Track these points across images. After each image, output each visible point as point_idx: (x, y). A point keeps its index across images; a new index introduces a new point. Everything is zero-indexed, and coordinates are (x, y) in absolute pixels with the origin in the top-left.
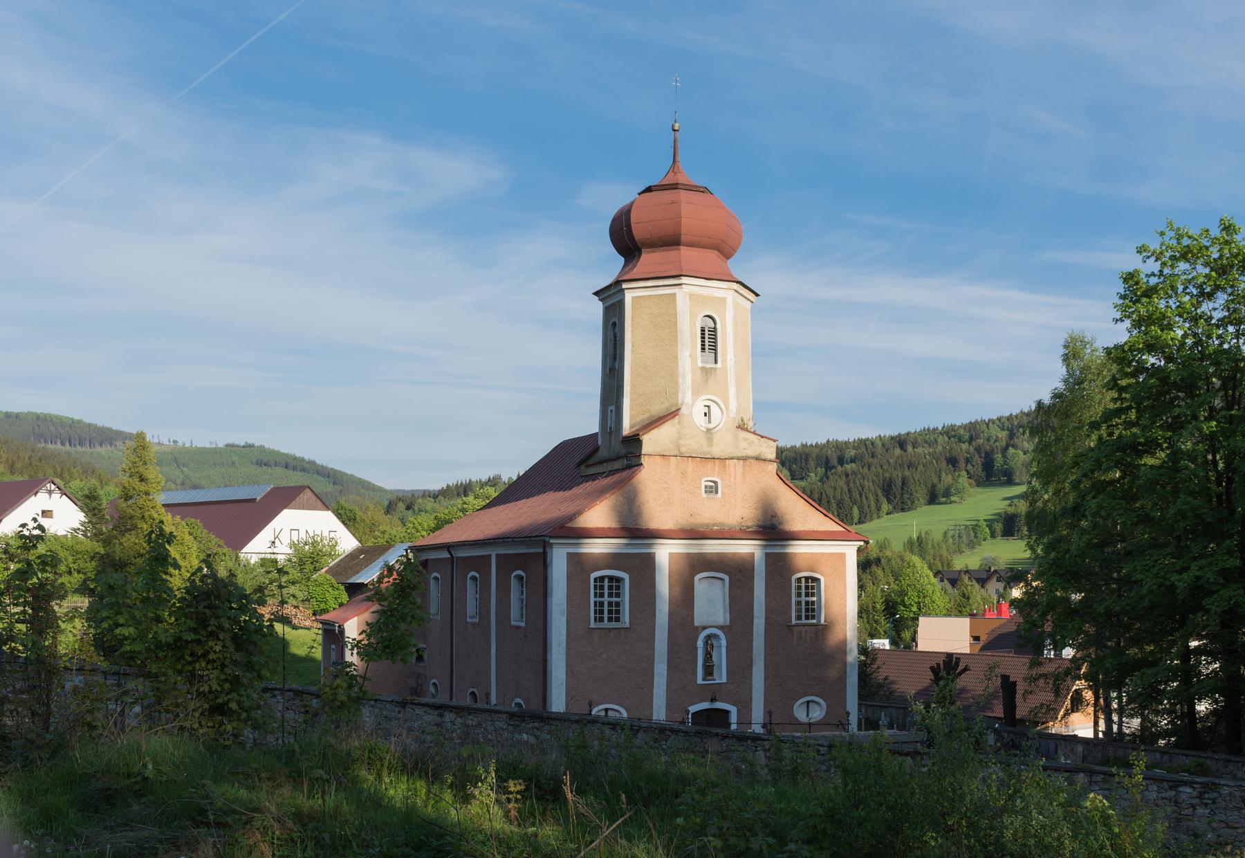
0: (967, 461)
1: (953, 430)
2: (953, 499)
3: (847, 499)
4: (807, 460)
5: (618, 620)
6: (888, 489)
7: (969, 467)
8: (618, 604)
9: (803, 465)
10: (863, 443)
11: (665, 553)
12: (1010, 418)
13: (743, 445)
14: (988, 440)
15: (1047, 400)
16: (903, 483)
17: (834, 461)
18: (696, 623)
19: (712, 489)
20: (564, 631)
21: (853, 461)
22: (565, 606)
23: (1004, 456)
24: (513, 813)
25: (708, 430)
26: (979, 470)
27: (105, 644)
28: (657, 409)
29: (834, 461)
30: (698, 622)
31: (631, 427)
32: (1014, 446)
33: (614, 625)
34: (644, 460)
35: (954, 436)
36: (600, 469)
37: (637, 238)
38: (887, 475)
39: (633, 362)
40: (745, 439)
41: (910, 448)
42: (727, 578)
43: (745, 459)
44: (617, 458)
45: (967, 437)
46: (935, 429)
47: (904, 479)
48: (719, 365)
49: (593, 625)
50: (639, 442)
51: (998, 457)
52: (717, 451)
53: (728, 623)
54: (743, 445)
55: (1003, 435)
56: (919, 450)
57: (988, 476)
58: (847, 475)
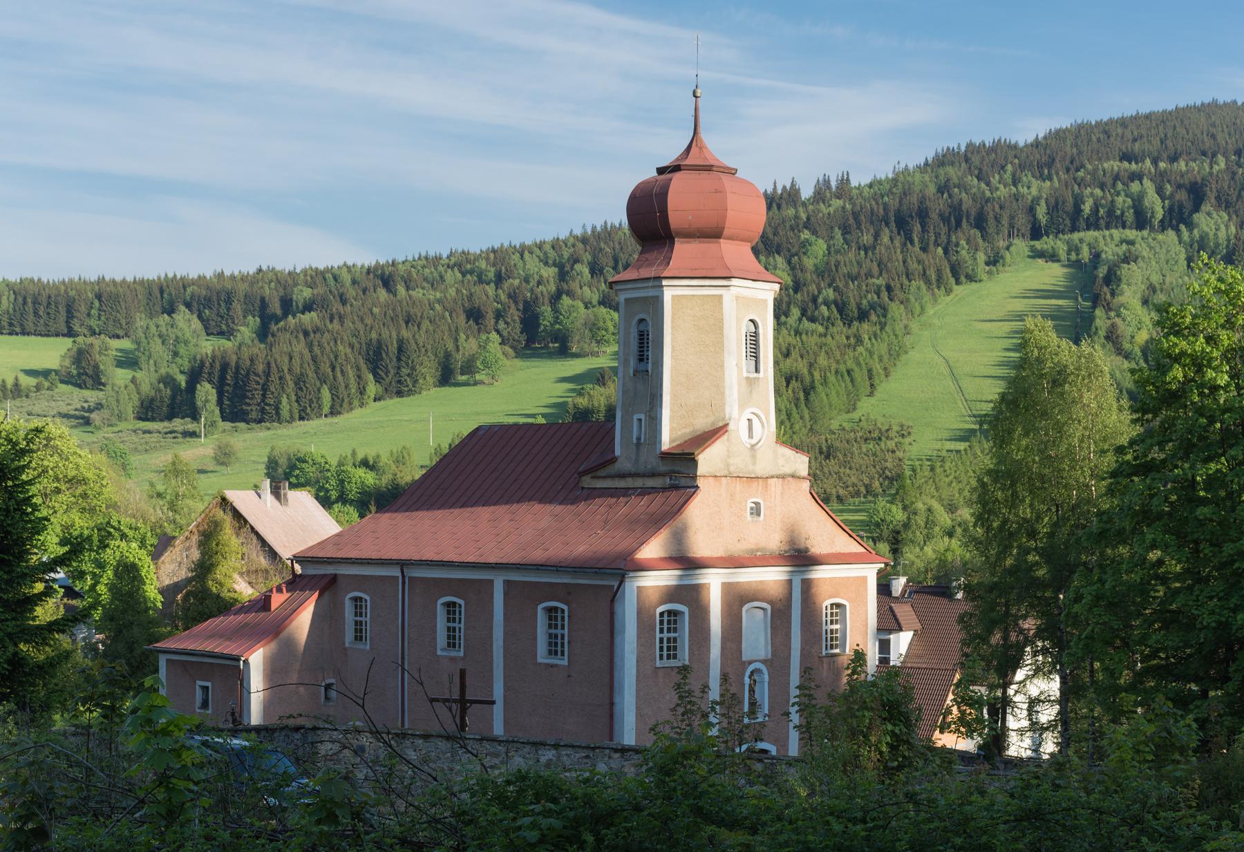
0: (499, 315)
1: (468, 261)
2: (478, 377)
3: (311, 374)
4: (229, 301)
5: (675, 657)
6: (375, 358)
7: (501, 325)
8: (550, 626)
9: (223, 310)
10: (317, 277)
11: (714, 582)
12: (555, 244)
13: (781, 461)
14: (527, 281)
16: (400, 349)
17: (276, 307)
18: (744, 659)
19: (756, 511)
20: (634, 672)
21: (308, 307)
23: (556, 311)
25: (753, 446)
26: (514, 328)
28: (702, 423)
29: (276, 307)
30: (746, 657)
31: (671, 442)
32: (570, 294)
33: (672, 663)
34: (700, 482)
35: (471, 272)
36: (629, 483)
37: (672, 227)
38: (374, 335)
39: (674, 368)
40: (783, 456)
41: (401, 289)
43: (783, 477)
44: (653, 475)
45: (491, 275)
46: (438, 259)
47: (331, 321)
48: (761, 375)
49: (658, 664)
50: (694, 462)
51: (546, 310)
52: (761, 468)
54: (781, 461)
55: (550, 273)
56: (417, 294)
57: (530, 341)
58: (306, 334)
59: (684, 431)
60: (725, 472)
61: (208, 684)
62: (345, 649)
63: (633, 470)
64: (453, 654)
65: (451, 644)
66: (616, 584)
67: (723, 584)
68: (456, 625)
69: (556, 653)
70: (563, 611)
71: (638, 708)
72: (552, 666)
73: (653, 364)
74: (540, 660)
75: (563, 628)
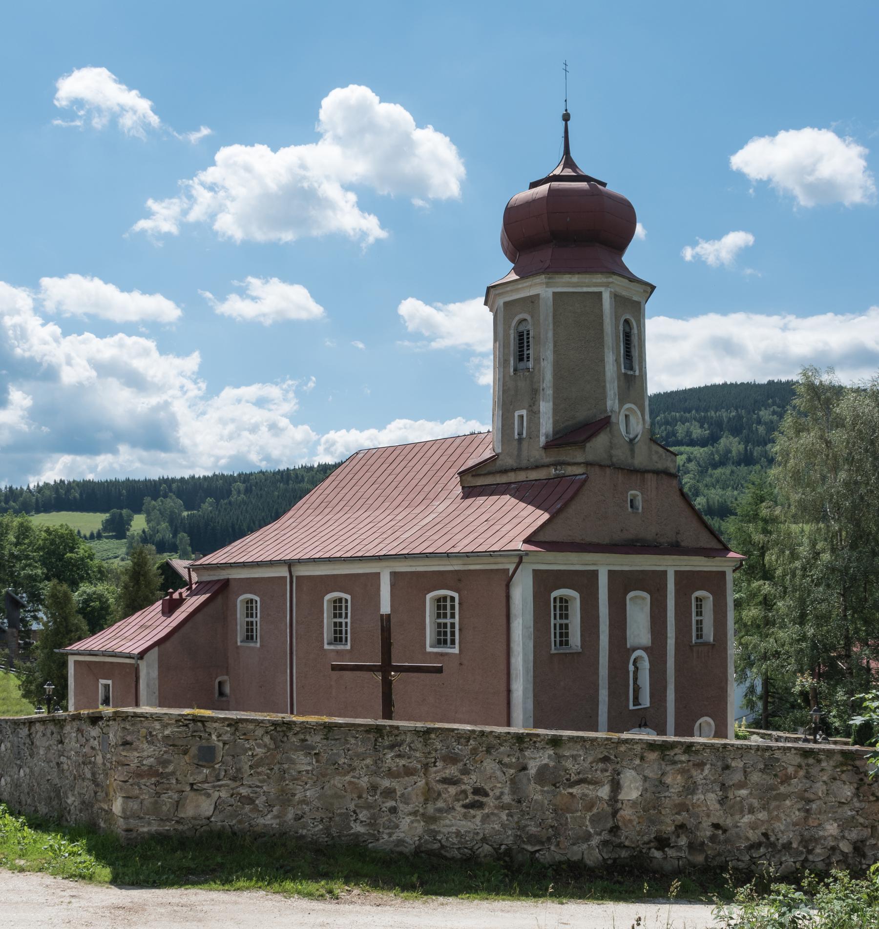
8: (439, 616)
13: (655, 458)
15: (197, 476)
22: (532, 630)
24: (620, 878)
43: (657, 472)
44: (537, 467)
49: (553, 651)
53: (650, 644)
62: (238, 647)
63: (515, 465)
64: (340, 647)
65: (338, 638)
66: (512, 568)
67: (609, 571)
68: (343, 620)
69: (445, 642)
73: (535, 360)
74: (429, 649)
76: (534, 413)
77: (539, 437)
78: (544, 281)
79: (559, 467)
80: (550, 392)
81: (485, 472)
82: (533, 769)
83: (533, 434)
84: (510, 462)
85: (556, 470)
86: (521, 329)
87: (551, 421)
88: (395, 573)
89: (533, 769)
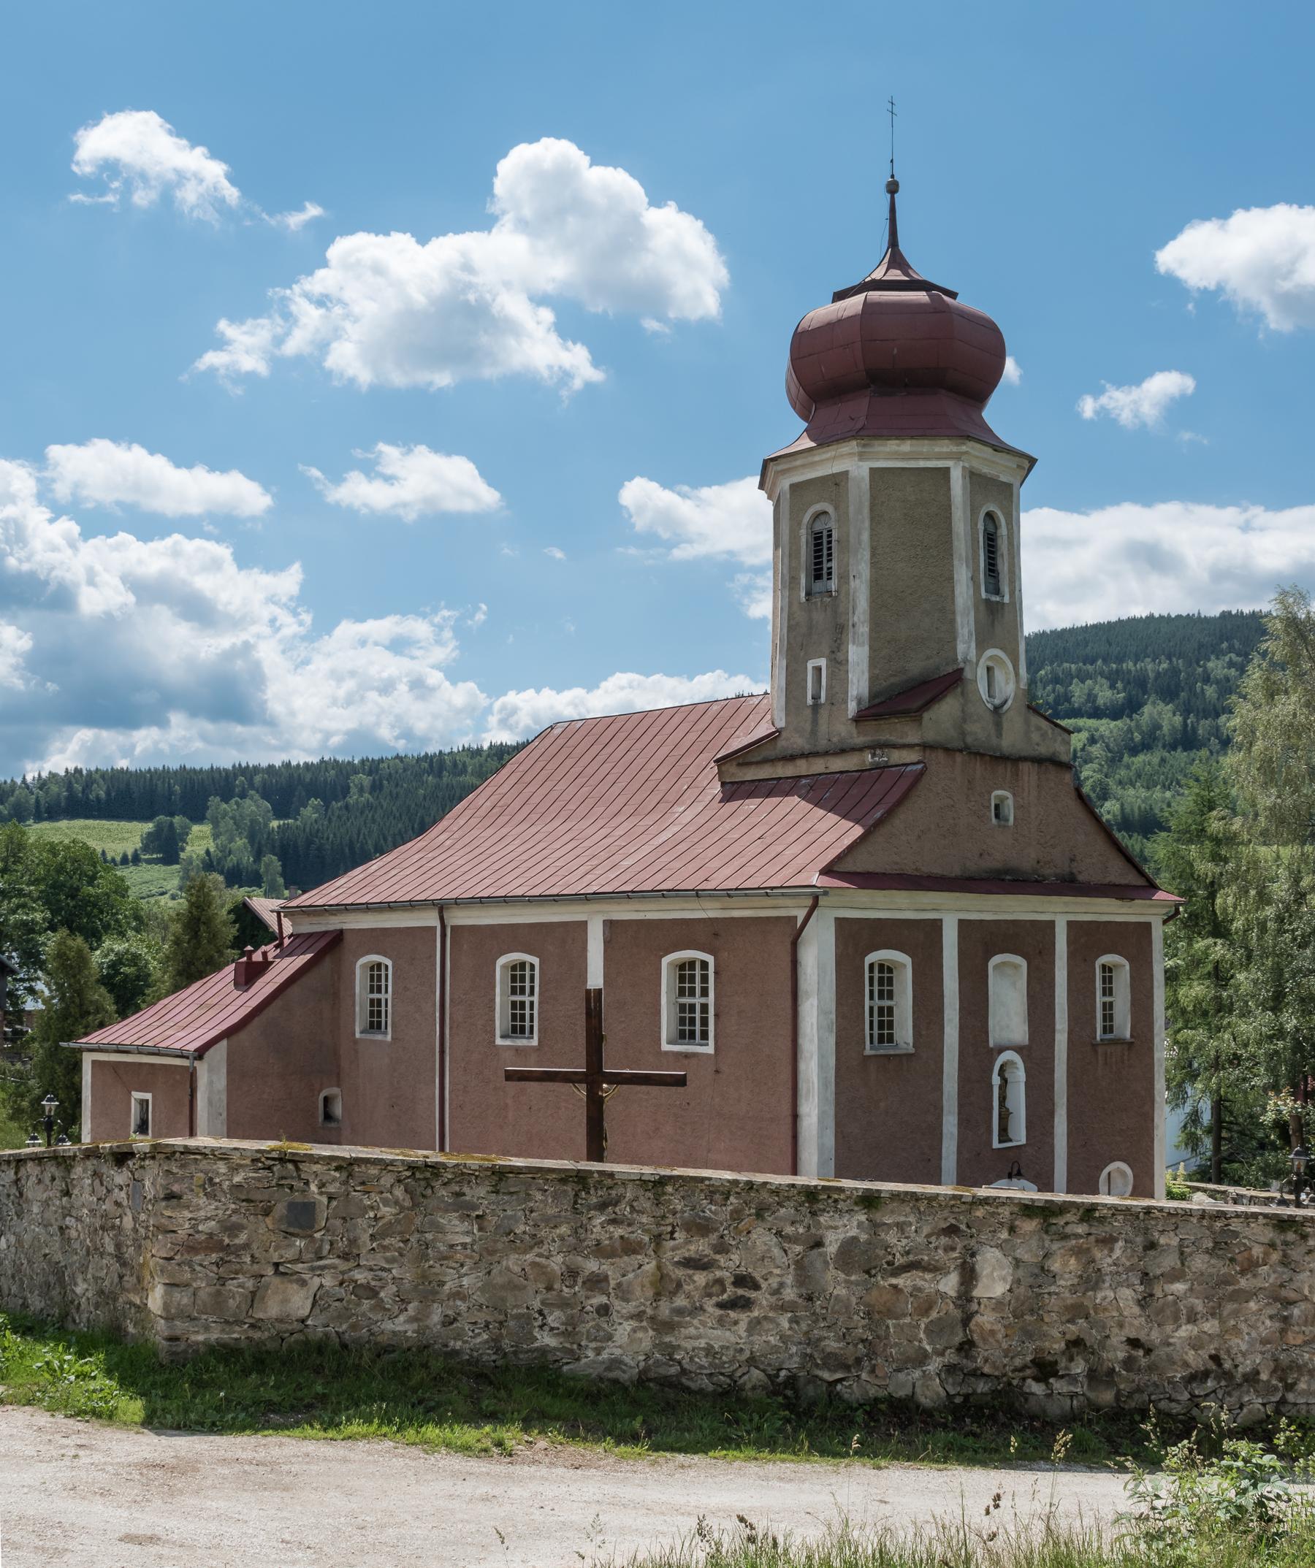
5: (891, 1039)
8: (682, 992)
13: (1035, 737)
27: (166, 1306)
33: (886, 1050)
42: (1022, 963)
44: (843, 751)
53: (1027, 1042)
54: (1035, 737)
59: (893, 680)
60: (960, 744)
61: (148, 1096)
62: (356, 1042)
64: (521, 1042)
65: (518, 1029)
66: (801, 914)
67: (960, 921)
68: (526, 999)
70: (704, 965)
71: (838, 1125)
72: (687, 1056)
73: (840, 577)
74: (666, 1047)
75: (705, 992)
76: (838, 663)
77: (846, 702)
78: (856, 449)
79: (878, 752)
80: (864, 629)
81: (759, 759)
82: (832, 1244)
83: (838, 697)
84: (798, 742)
85: (874, 755)
86: (818, 527)
87: (866, 676)
88: (611, 922)
89: (832, 1244)
